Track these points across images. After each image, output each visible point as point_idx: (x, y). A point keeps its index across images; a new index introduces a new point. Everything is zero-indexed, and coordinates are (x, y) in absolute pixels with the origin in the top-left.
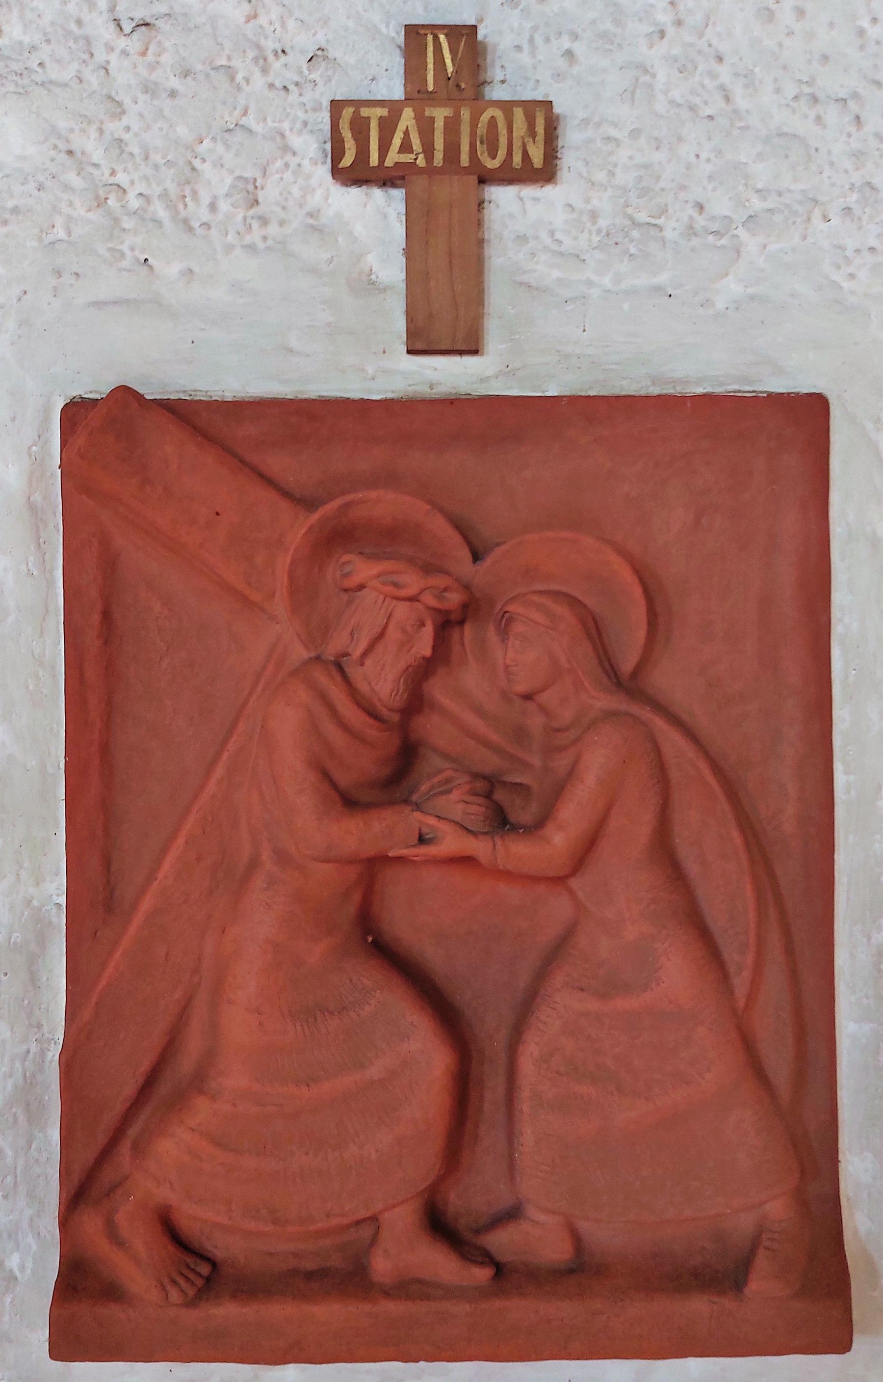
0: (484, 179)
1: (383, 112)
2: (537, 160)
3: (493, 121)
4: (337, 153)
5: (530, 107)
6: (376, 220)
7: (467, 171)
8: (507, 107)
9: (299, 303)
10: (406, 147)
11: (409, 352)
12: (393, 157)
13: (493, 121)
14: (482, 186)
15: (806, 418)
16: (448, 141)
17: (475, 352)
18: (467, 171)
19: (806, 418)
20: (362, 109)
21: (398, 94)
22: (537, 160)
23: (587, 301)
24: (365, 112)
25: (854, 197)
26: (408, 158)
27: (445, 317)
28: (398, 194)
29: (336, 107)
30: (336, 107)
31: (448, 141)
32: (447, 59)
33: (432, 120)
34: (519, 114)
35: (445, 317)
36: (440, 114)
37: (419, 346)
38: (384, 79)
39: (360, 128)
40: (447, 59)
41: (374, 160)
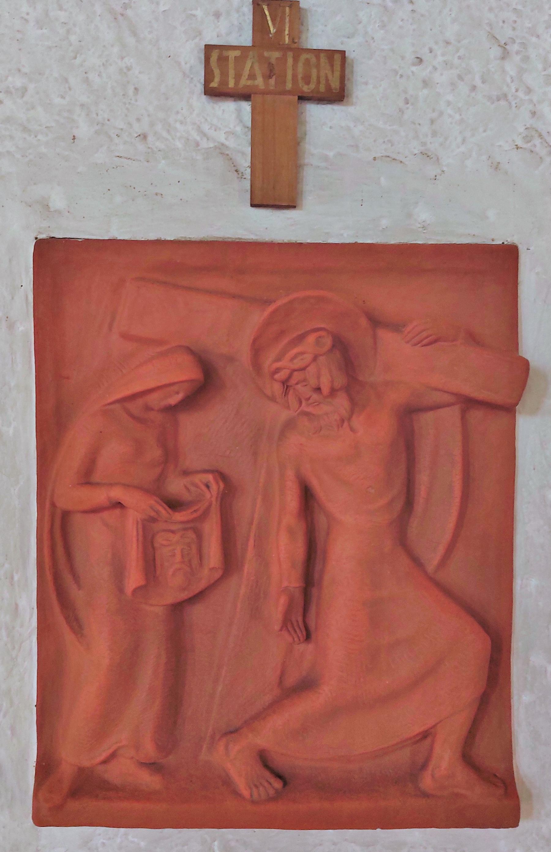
0: (302, 98)
1: (237, 53)
5: (331, 54)
6: (232, 120)
7: (290, 93)
9: (176, 176)
10: (252, 76)
11: (253, 205)
12: (244, 81)
13: (307, 61)
14: (300, 101)
15: (503, 260)
16: (279, 75)
17: (294, 207)
18: (290, 93)
19: (503, 260)
20: (230, 86)
22: (335, 84)
23: (361, 188)
24: (225, 53)
25: (535, 99)
26: (249, 83)
27: (274, 188)
28: (246, 107)
29: (209, 48)
31: (279, 75)
33: (227, 58)
34: (323, 59)
35: (274, 188)
37: (256, 202)
39: (223, 60)
41: (231, 84)
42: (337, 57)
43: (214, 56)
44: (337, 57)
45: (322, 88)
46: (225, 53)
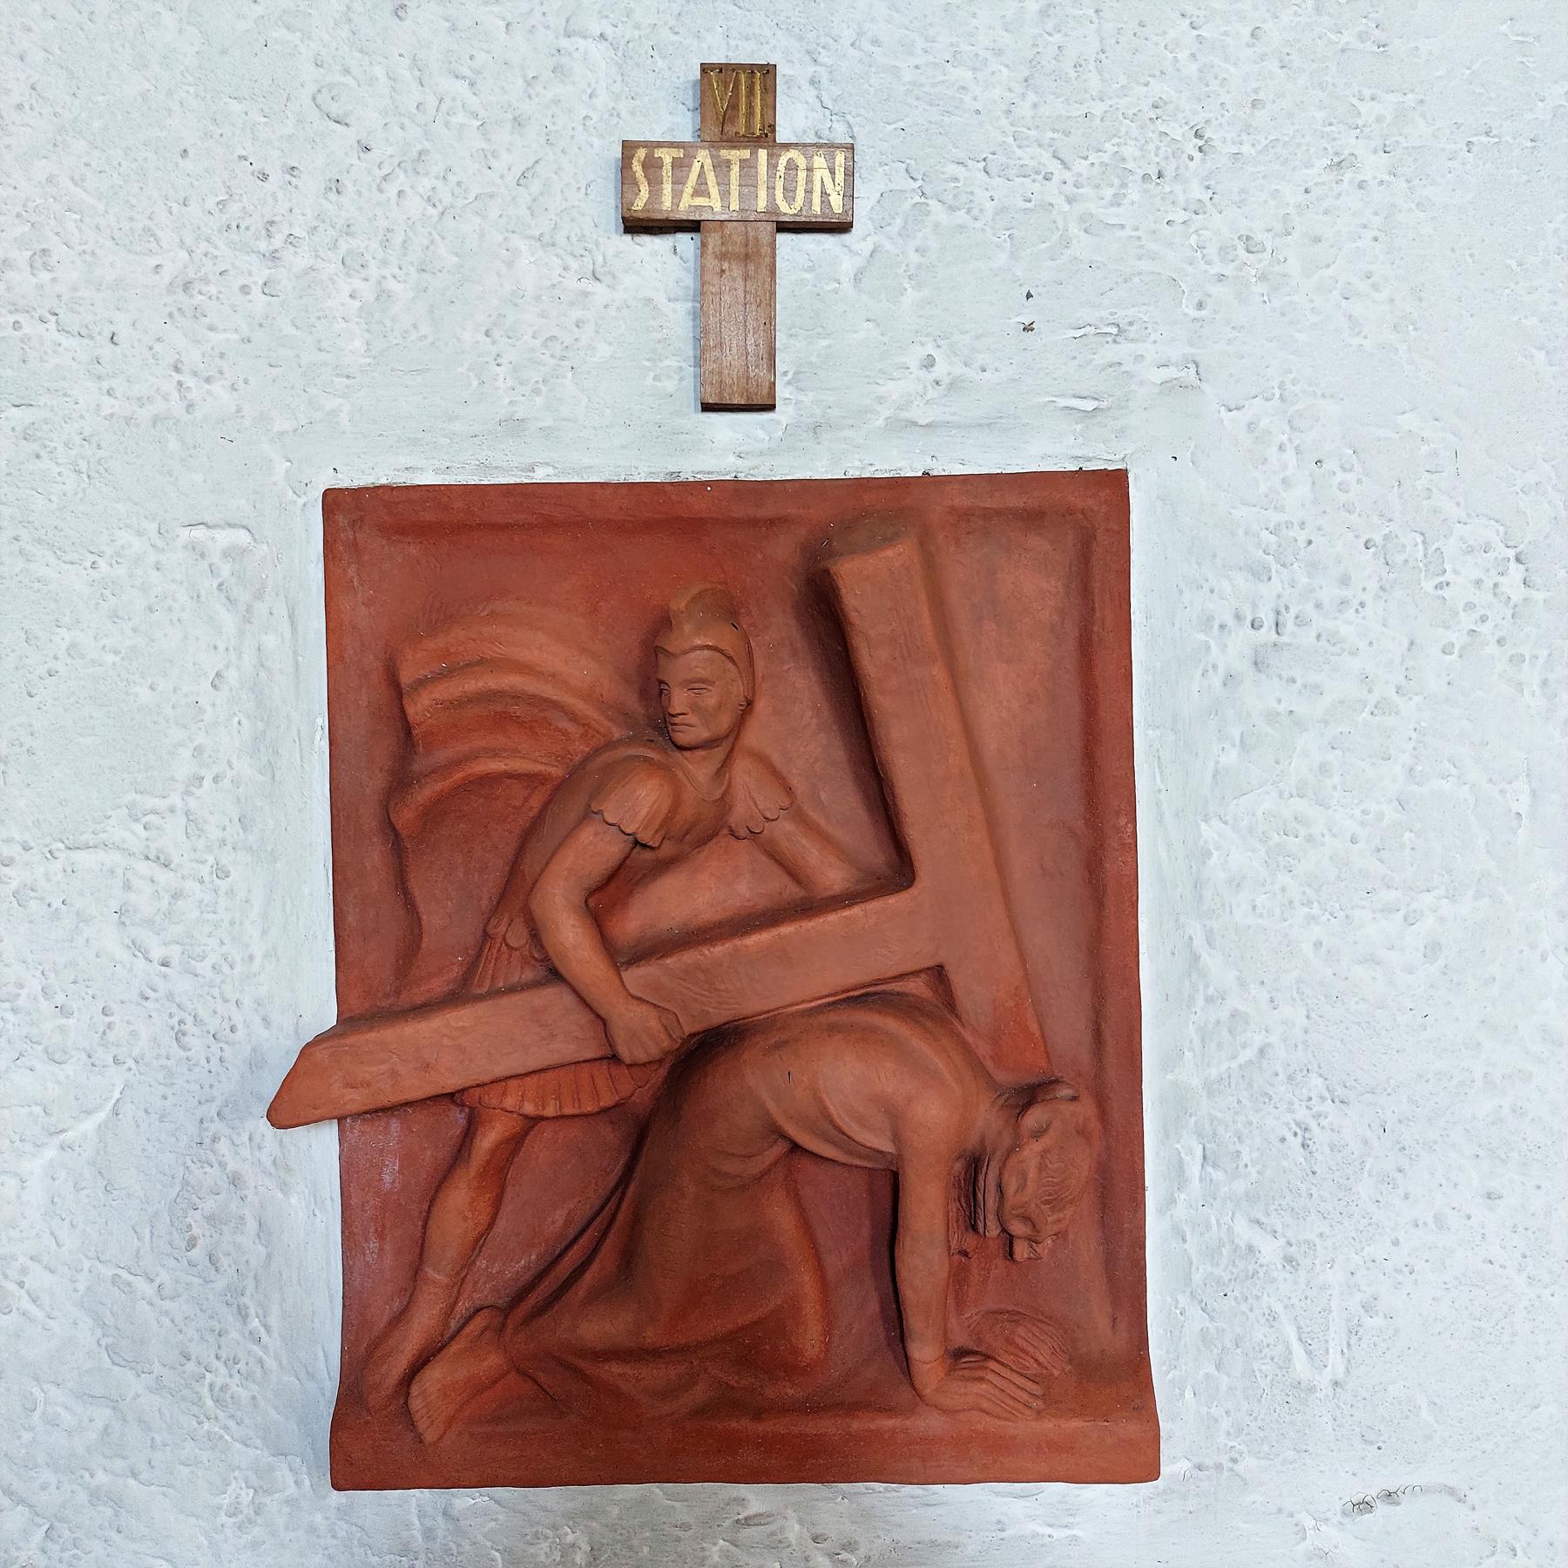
2: (837, 203)
4: (625, 203)
9: (590, 391)
13: (792, 166)
21: (687, 136)
24: (658, 153)
28: (685, 241)
29: (628, 147)
30: (628, 147)
31: (724, 175)
32: (737, 101)
38: (671, 119)
40: (737, 101)
41: (667, 203)
42: (840, 158)
43: (641, 153)
45: (817, 208)
46: (658, 153)
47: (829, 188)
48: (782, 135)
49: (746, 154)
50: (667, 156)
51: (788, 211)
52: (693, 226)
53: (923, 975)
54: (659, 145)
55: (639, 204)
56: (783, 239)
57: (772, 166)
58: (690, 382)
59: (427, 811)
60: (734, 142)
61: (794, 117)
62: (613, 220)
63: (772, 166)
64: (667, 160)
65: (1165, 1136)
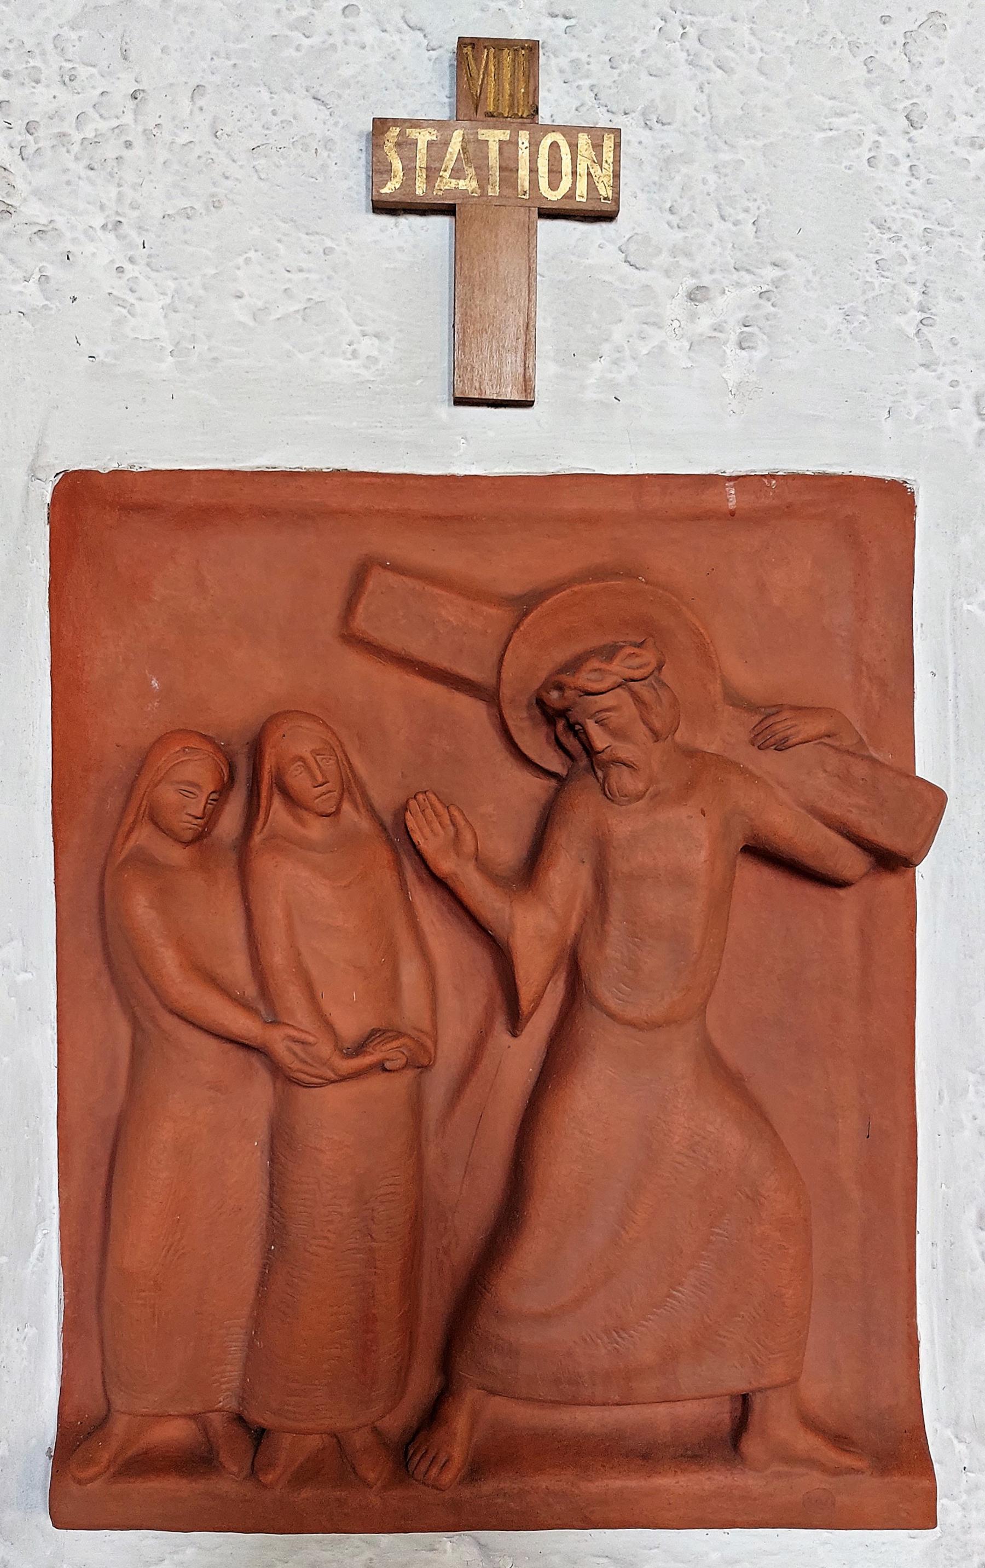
2: (604, 191)
3: (553, 186)
4: (379, 170)
5: (597, 135)
8: (571, 132)
9: (328, 369)
13: (554, 146)
16: (485, 164)
21: (443, 112)
22: (604, 191)
23: (643, 383)
28: (442, 223)
29: (380, 125)
30: (380, 125)
31: (485, 164)
32: (495, 75)
33: (415, 143)
36: (494, 137)
38: (426, 93)
40: (495, 75)
42: (608, 144)
43: (394, 132)
44: (608, 144)
46: (413, 133)
47: (595, 171)
48: (544, 116)
49: (504, 135)
50: (423, 137)
51: (553, 196)
52: (448, 210)
53: (494, 681)
54: (416, 124)
55: (390, 188)
56: (544, 226)
57: (534, 146)
58: (363, 191)
59: (151, 820)
60: (494, 118)
61: (554, 103)
62: (363, 201)
63: (534, 146)
64: (422, 145)
65: (317, 1541)
